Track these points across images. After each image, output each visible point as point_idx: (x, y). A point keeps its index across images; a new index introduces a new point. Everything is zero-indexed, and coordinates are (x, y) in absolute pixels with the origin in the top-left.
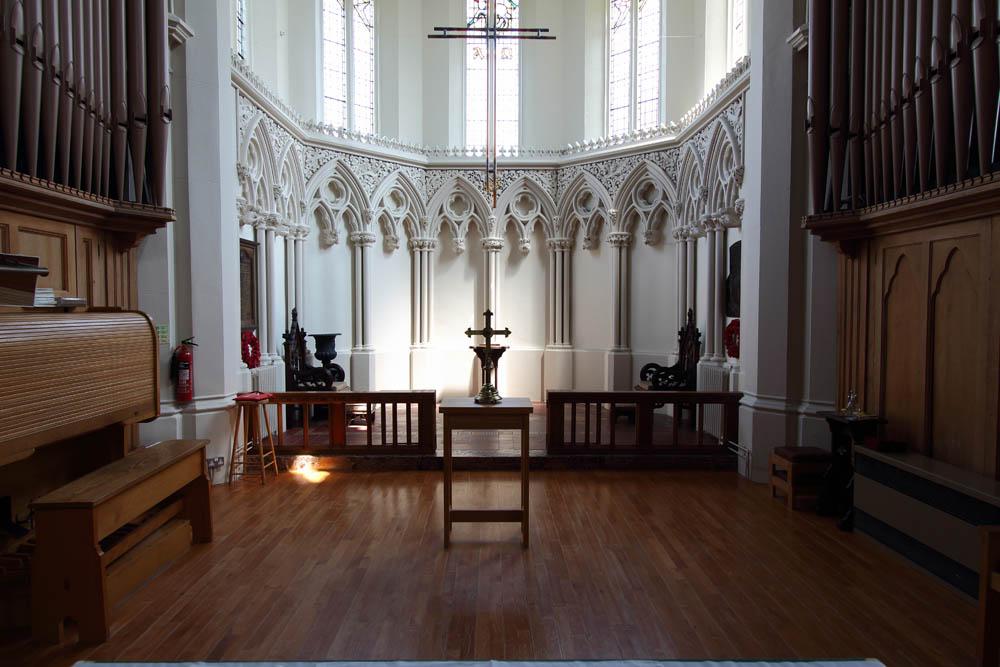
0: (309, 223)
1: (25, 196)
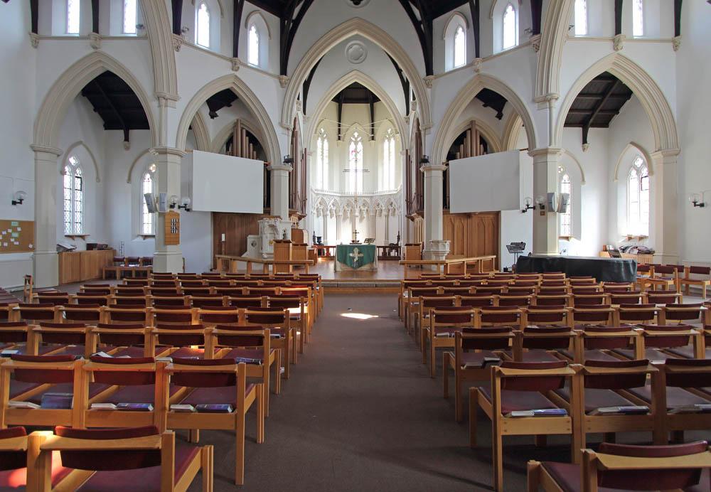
0: (315, 212)
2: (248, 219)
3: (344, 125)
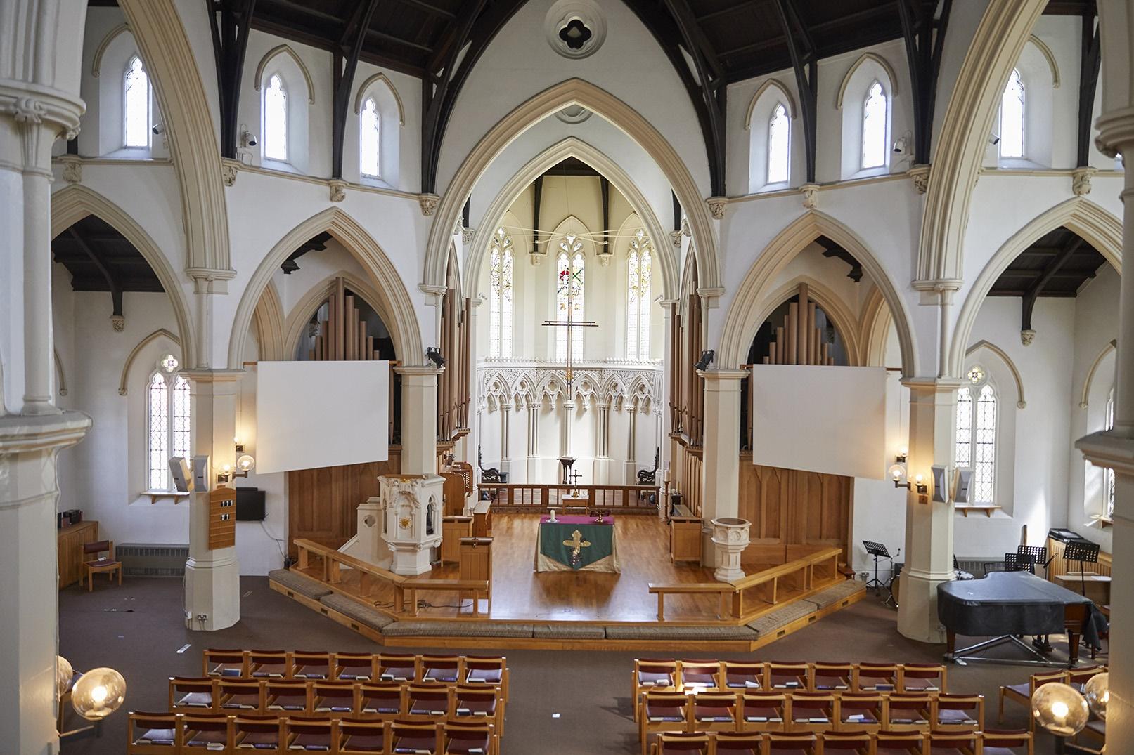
1: (564, 652)
2: (360, 481)
3: (547, 218)
